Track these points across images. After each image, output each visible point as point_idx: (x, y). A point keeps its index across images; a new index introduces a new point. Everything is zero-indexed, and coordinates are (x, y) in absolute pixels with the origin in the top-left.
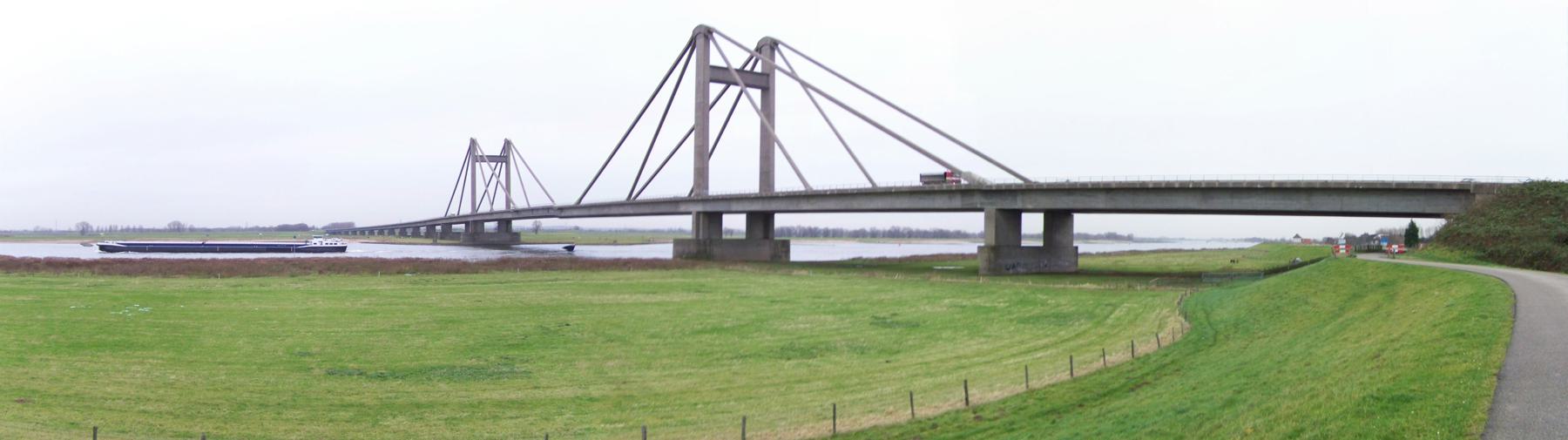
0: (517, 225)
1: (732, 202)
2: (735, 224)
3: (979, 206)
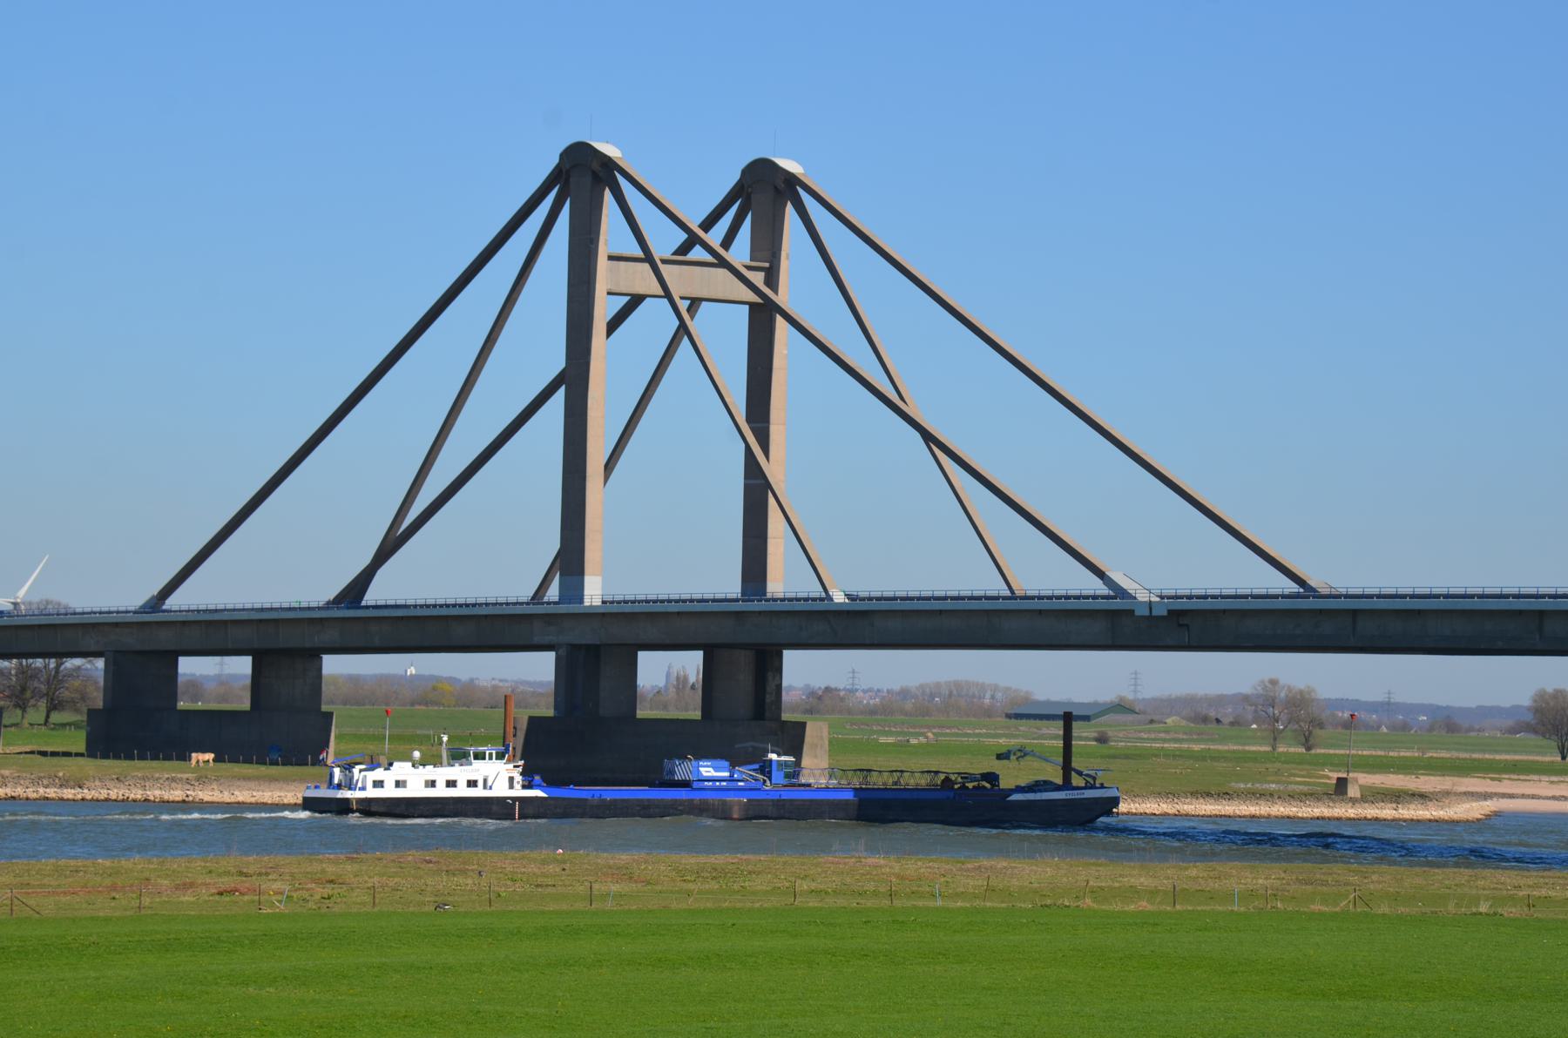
3: (536, 640)
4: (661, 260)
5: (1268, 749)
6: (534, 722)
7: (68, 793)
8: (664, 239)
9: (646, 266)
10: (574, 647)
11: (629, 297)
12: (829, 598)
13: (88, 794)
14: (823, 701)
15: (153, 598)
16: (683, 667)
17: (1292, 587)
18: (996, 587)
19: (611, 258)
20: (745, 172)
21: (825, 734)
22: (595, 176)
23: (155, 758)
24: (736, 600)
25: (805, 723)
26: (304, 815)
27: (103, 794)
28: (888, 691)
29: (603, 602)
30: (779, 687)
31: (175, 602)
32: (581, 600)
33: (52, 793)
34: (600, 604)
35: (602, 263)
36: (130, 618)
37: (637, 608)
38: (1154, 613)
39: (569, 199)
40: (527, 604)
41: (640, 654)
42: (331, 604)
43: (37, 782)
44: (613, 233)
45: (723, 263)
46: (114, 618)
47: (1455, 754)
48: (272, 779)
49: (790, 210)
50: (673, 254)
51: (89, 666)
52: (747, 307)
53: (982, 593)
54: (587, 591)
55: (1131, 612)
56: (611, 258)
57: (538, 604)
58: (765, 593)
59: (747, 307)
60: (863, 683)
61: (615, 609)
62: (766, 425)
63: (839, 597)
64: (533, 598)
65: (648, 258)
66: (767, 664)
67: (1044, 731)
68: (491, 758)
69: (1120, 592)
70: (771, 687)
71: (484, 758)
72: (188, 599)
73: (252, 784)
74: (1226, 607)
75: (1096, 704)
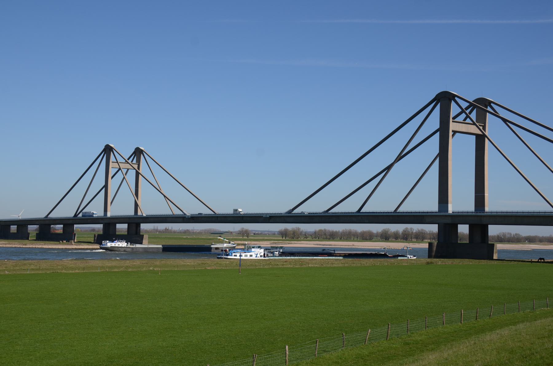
0: (494, 230)
1: (461, 218)
2: (463, 229)
3: (100, 222)
4: (463, 121)
5: (242, 238)
6: (99, 235)
7: (24, 246)
8: (120, 160)
9: (117, 163)
10: (106, 223)
11: (438, 133)
12: (143, 215)
13: (27, 246)
14: (147, 232)
15: (291, 210)
16: (193, 227)
17: (213, 213)
18: (172, 214)
19: (112, 162)
20: (135, 149)
21: (147, 236)
22: (110, 149)
23: (42, 241)
24: (436, 212)
25: (143, 235)
26: (101, 251)
27: (29, 246)
28: (200, 230)
29: (452, 212)
30: (140, 229)
31: (50, 216)
32: (447, 211)
33: (21, 246)
34: (452, 213)
35: (111, 163)
36: (42, 219)
37: (228, 215)
38: (267, 216)
39: (439, 103)
40: (393, 213)
41: (458, 225)
42: (44, 218)
43: (19, 245)
44: (112, 158)
45: (128, 163)
46: (38, 219)
47: (277, 238)
48: (56, 244)
49: (142, 155)
50: (463, 121)
51: (54, 227)
52: (474, 137)
53: (259, 213)
54: (108, 214)
55: (185, 217)
56: (112, 162)
57: (396, 213)
58: (484, 210)
59: (474, 137)
60: (195, 228)
61: (112, 217)
62: (136, 188)
63: (144, 215)
64: (394, 211)
65: (117, 162)
66: (138, 225)
67: (215, 236)
68: (256, 248)
69: (185, 214)
70: (138, 229)
71: (258, 247)
72: (52, 216)
73: (52, 245)
74: (520, 215)
75: (223, 231)
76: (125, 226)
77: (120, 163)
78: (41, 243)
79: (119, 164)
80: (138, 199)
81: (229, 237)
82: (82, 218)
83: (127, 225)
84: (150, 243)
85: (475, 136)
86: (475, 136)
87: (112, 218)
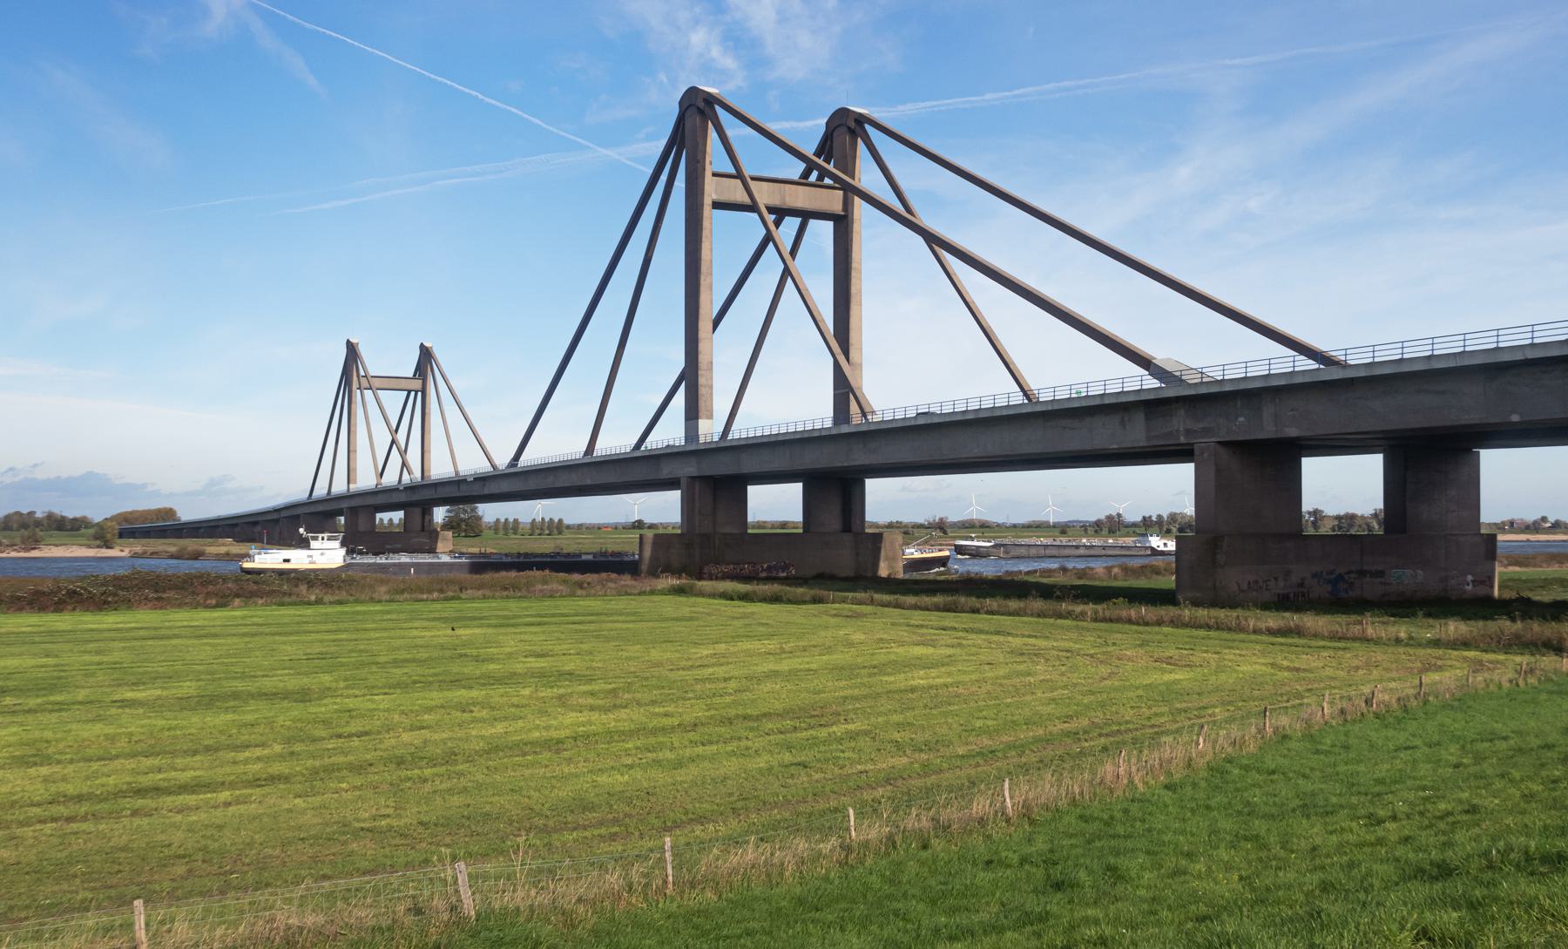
19: (715, 175)
56: (715, 175)
65: (739, 175)
76: (397, 516)
77: (753, 179)
78: (549, 560)
79: (753, 185)
80: (846, 353)
81: (298, 613)
82: (834, 432)
83: (796, 489)
84: (1500, 573)
85: (831, 223)
86: (831, 223)
87: (726, 448)
